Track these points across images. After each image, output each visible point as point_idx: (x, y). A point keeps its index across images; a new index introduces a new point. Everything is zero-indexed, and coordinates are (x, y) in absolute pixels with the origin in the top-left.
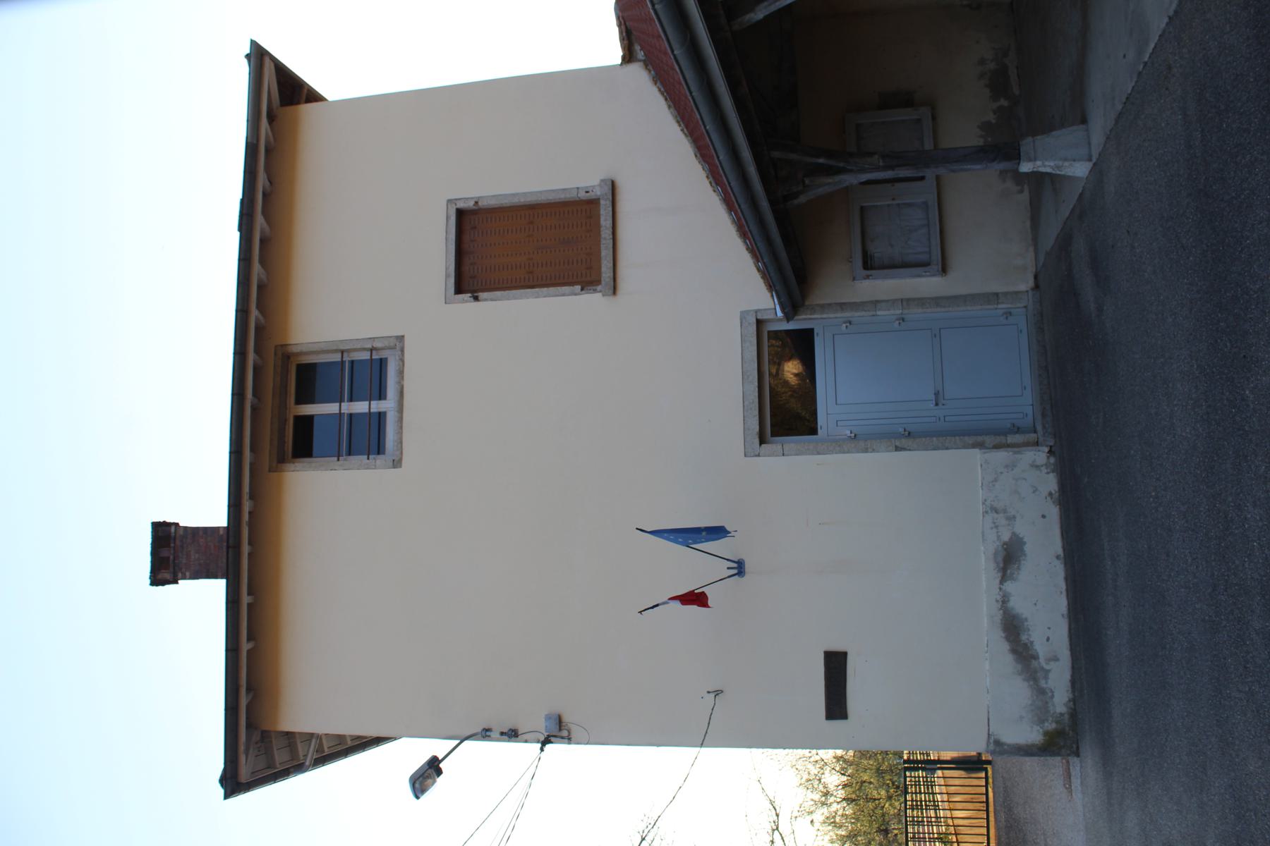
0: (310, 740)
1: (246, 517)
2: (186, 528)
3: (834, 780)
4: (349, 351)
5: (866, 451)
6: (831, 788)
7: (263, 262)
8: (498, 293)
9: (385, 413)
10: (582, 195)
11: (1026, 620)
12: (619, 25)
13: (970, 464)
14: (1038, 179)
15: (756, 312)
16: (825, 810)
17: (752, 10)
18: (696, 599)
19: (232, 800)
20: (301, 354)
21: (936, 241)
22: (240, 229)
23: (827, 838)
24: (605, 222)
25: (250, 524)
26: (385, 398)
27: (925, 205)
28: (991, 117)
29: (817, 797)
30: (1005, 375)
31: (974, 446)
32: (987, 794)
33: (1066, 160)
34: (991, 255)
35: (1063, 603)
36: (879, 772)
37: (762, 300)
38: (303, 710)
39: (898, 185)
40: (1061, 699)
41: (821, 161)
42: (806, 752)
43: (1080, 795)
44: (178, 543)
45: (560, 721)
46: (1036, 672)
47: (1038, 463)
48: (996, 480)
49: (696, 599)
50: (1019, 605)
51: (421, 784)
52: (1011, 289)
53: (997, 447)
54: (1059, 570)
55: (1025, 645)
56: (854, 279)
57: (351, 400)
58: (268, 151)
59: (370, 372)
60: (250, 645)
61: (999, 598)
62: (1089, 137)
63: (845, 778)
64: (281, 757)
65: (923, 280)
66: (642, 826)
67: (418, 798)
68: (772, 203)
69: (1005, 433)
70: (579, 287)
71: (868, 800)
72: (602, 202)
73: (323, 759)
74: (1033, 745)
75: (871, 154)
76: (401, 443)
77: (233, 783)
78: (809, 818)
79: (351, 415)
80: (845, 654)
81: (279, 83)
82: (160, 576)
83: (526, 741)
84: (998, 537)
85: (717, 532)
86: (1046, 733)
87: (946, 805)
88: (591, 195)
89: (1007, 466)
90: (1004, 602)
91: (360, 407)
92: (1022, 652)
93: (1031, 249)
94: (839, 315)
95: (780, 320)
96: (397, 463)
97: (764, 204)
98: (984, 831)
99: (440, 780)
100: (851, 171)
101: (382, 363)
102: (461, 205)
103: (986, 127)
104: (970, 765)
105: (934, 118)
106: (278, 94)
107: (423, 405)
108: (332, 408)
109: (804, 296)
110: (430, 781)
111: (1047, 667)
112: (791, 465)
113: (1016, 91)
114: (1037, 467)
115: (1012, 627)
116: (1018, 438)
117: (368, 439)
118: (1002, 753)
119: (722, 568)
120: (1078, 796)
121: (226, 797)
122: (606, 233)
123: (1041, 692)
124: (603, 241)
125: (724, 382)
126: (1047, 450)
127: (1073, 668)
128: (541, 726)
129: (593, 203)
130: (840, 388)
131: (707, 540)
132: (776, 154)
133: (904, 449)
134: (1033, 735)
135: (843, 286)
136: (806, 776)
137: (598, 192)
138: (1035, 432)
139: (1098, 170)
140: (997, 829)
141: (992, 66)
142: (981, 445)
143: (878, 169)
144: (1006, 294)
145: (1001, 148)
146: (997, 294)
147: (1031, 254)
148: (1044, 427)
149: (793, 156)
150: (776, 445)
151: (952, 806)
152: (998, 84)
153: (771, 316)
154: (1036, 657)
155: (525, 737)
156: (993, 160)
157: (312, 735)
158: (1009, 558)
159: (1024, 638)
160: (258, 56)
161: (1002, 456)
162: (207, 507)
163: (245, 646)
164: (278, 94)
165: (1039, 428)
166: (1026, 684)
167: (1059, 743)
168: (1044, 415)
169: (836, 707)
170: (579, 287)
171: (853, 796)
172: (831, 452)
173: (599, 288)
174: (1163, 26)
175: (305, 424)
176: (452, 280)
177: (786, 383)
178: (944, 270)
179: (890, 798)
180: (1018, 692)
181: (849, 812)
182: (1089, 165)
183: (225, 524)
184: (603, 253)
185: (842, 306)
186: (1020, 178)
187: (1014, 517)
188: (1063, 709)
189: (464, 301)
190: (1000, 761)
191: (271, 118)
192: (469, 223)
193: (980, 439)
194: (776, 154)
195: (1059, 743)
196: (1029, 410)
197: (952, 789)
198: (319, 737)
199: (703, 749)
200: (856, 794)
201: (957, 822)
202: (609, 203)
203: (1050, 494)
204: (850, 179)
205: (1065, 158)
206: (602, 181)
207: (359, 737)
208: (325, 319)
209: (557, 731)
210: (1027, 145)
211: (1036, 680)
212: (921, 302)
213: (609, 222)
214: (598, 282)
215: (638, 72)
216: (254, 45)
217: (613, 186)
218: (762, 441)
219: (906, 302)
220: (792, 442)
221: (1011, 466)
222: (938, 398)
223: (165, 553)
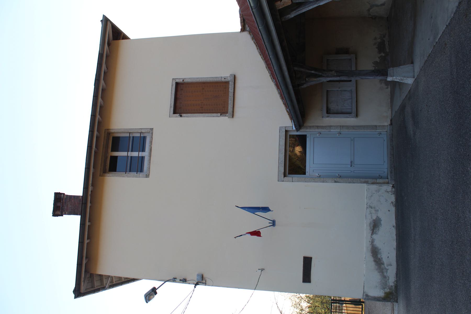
0: (108, 278)
1: (90, 193)
2: (67, 195)
3: (305, 305)
4: (132, 133)
5: (323, 182)
6: (304, 308)
9: (144, 157)
10: (223, 80)
12: (241, 18)
13: (363, 189)
14: (394, 84)
17: (289, 14)
18: (256, 233)
22: (95, 85)
24: (231, 90)
26: (145, 151)
27: (351, 91)
28: (378, 60)
30: (377, 157)
31: (364, 182)
33: (405, 77)
34: (375, 111)
35: (395, 244)
36: (322, 303)
37: (288, 123)
39: (342, 83)
40: (392, 280)
41: (313, 72)
42: (295, 294)
44: (64, 201)
45: (202, 277)
46: (383, 269)
47: (388, 190)
48: (372, 196)
49: (256, 233)
50: (378, 244)
51: (149, 297)
52: (381, 124)
53: (373, 183)
54: (394, 231)
56: (323, 117)
57: (132, 151)
58: (107, 56)
59: (140, 141)
60: (88, 241)
61: (370, 240)
62: (414, 69)
63: (309, 304)
64: (97, 284)
67: (147, 302)
68: (293, 87)
69: (376, 178)
70: (219, 114)
72: (230, 83)
73: (113, 286)
74: (380, 297)
75: (331, 71)
76: (150, 168)
77: (78, 293)
79: (131, 157)
80: (311, 258)
81: (113, 31)
82: (56, 213)
83: (189, 284)
84: (372, 217)
85: (266, 209)
86: (385, 293)
88: (226, 80)
90: (372, 242)
91: (135, 154)
92: (378, 262)
93: (390, 110)
94: (316, 130)
95: (294, 131)
96: (147, 176)
99: (156, 296)
100: (324, 76)
101: (144, 138)
102: (178, 81)
103: (376, 63)
104: (356, 302)
105: (356, 59)
106: (112, 35)
107: (159, 154)
108: (124, 154)
109: (304, 122)
110: (152, 296)
111: (387, 268)
112: (295, 185)
113: (388, 50)
114: (388, 192)
115: (375, 252)
116: (381, 181)
117: (137, 166)
118: (368, 299)
119: (267, 223)
121: (75, 298)
122: (231, 95)
123: (385, 277)
124: (230, 97)
125: (272, 153)
126: (392, 186)
127: (397, 269)
128: (195, 278)
129: (227, 83)
130: (315, 158)
132: (296, 68)
133: (338, 182)
134: (380, 293)
135: (319, 119)
136: (294, 303)
137: (229, 79)
138: (388, 179)
139: (417, 81)
141: (379, 40)
142: (367, 182)
143: (334, 76)
144: (379, 126)
145: (381, 71)
146: (376, 126)
147: (390, 112)
148: (391, 177)
149: (302, 70)
150: (290, 178)
152: (381, 47)
153: (291, 129)
154: (383, 264)
155: (189, 282)
157: (109, 276)
158: (375, 225)
159: (379, 256)
161: (374, 187)
162: (75, 188)
163: (86, 241)
164: (112, 35)
165: (389, 177)
167: (390, 297)
168: (391, 173)
169: (307, 278)
170: (219, 114)
173: (227, 115)
174: (444, 28)
175: (114, 159)
176: (172, 109)
178: (357, 116)
180: (376, 277)
182: (413, 79)
184: (229, 102)
185: (318, 127)
186: (387, 83)
188: (393, 284)
189: (176, 117)
190: (367, 302)
191: (109, 44)
192: (180, 88)
193: (367, 180)
194: (296, 68)
195: (390, 297)
196: (386, 170)
198: (112, 277)
199: (257, 292)
202: (233, 83)
203: (392, 202)
205: (404, 76)
207: (127, 278)
208: (123, 121)
209: (201, 280)
210: (390, 70)
211: (383, 273)
212: (348, 127)
213: (232, 91)
214: (227, 113)
215: (246, 35)
216: (104, 16)
218: (285, 176)
219: (342, 127)
220: (296, 177)
222: (352, 164)
223: (59, 204)
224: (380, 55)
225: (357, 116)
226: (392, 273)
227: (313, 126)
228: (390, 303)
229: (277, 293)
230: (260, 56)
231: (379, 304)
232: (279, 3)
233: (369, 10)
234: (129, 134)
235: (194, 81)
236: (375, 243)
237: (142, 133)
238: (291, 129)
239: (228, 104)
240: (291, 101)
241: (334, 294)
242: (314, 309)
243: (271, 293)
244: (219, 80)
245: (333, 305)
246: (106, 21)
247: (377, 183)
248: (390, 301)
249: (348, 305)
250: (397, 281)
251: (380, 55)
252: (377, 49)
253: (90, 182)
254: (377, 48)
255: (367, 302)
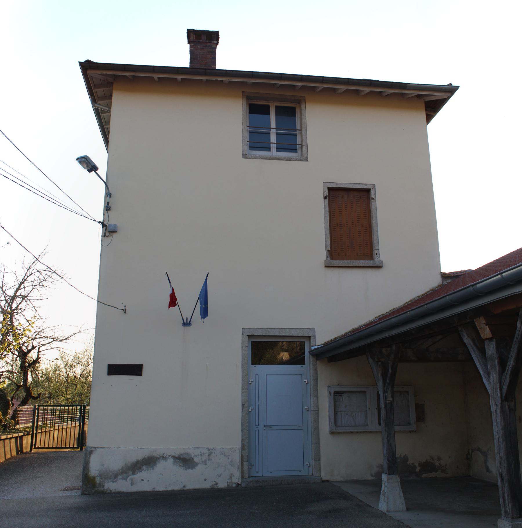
0: (108, 107)
1: (220, 79)
2: (216, 48)
3: (78, 370)
4: (301, 133)
6: (74, 369)
7: (347, 91)
8: (327, 209)
9: (270, 151)
10: (375, 252)
11: (153, 469)
12: (461, 272)
13: (234, 442)
15: (314, 336)
16: (63, 366)
18: (173, 301)
19: (78, 67)
20: (301, 109)
21: (347, 429)
22: (364, 80)
23: (48, 366)
24: (362, 263)
25: (217, 81)
26: (277, 151)
28: (410, 462)
29: (70, 362)
30: (280, 462)
31: (243, 444)
32: (65, 448)
33: (388, 499)
35: (160, 488)
36: (80, 394)
37: (321, 339)
38: (122, 104)
39: (376, 412)
40: (111, 486)
41: (390, 371)
42: (92, 357)
43: (61, 495)
44: (208, 44)
46: (126, 473)
47: (233, 478)
49: (173, 301)
50: (161, 466)
51: (84, 161)
52: (322, 468)
53: (242, 456)
54: (177, 487)
55: (141, 468)
57: (277, 134)
58: (403, 94)
59: (291, 144)
60: (156, 79)
61: (165, 455)
63: (79, 376)
64: (100, 91)
65: (328, 422)
66: (59, 272)
67: (77, 159)
70: (329, 249)
71: (67, 388)
72: (372, 261)
73: (98, 113)
74: (89, 471)
75: (392, 396)
76: (255, 158)
77: (87, 67)
78: (59, 358)
79: (269, 133)
80: (141, 375)
81: (437, 100)
82: (192, 34)
83: (104, 215)
84: (196, 456)
85: (204, 313)
86: (94, 478)
87: (61, 427)
88: (375, 256)
89: (232, 461)
90: (163, 457)
91: (273, 138)
92: (137, 466)
93: (342, 479)
94: (312, 378)
95: (310, 348)
96: (245, 156)
97: (369, 341)
98: (46, 446)
99: (86, 171)
100: (384, 386)
101: (295, 150)
102: (372, 191)
103: (405, 459)
104: (81, 439)
105: (410, 432)
106: (431, 100)
107: (275, 171)
108: (273, 124)
110: (85, 166)
112: (236, 351)
113: (424, 476)
114: (231, 477)
115: (149, 462)
116: (246, 468)
117: (257, 142)
118: (86, 454)
119: (187, 315)
120: (61, 494)
121: (80, 63)
122: (356, 263)
124: (352, 261)
126: (239, 483)
127: (127, 493)
128: (112, 222)
129: (371, 257)
130: (275, 377)
131: (201, 308)
133: (243, 409)
135: (327, 378)
136: (81, 356)
137: (377, 260)
138: (249, 477)
139: (382, 515)
140: (47, 453)
141: (437, 464)
142: (243, 448)
143: (385, 400)
144: (320, 465)
145: (394, 464)
146: (319, 460)
147: (339, 479)
148: (251, 482)
151: (60, 430)
152: (427, 466)
153: (312, 344)
154: (134, 473)
155: (106, 214)
156: (388, 460)
157: (110, 108)
158: (185, 461)
159: (144, 467)
160: (451, 90)
161: (237, 458)
162: (226, 59)
163: (156, 76)
164: (431, 100)
165: (251, 479)
166: (120, 468)
167: (89, 484)
168: (257, 481)
169: (115, 370)
170: (329, 249)
171: (69, 380)
172: (243, 371)
173: (329, 259)
175: (265, 111)
176: (335, 186)
177: (279, 353)
178: (332, 433)
179: (67, 399)
180: (116, 463)
181: (61, 378)
182: (385, 510)
183: (217, 68)
184: (346, 261)
185: (316, 380)
186: (378, 475)
187: (206, 464)
188: (106, 487)
189: (324, 192)
191: (419, 96)
192: (362, 196)
195: (89, 484)
196: (260, 474)
197: (69, 430)
198: (109, 112)
199: (94, 304)
200: (70, 382)
201: (52, 432)
202: (371, 265)
203: (217, 484)
204: (380, 384)
205: (391, 498)
206: (382, 261)
207: (109, 132)
208: (318, 122)
209: (109, 230)
210: (396, 478)
211: (122, 473)
212: (317, 421)
213: (361, 265)
215: (437, 281)
216: (457, 88)
217: (380, 267)
218: (249, 336)
219: (317, 413)
220: (249, 351)
221: (232, 464)
223: (204, 37)
224: (417, 466)
225: (332, 433)
226: (121, 486)
227: (317, 373)
228: (81, 484)
229: (93, 331)
230: (410, 300)
231: (79, 470)
232: (484, 322)
233: (479, 449)
234: (300, 143)
235: (373, 214)
236: (162, 461)
237: (302, 147)
238: (312, 343)
239: (343, 260)
240: (350, 343)
241: (93, 410)
242: (73, 384)
243: (94, 326)
244: (375, 247)
245: (79, 407)
246: (450, 90)
247: (242, 463)
248: (82, 485)
249: (77, 429)
250: (110, 493)
251: (417, 466)
252: (425, 461)
253: (234, 79)
254: (427, 460)
255: (82, 454)
